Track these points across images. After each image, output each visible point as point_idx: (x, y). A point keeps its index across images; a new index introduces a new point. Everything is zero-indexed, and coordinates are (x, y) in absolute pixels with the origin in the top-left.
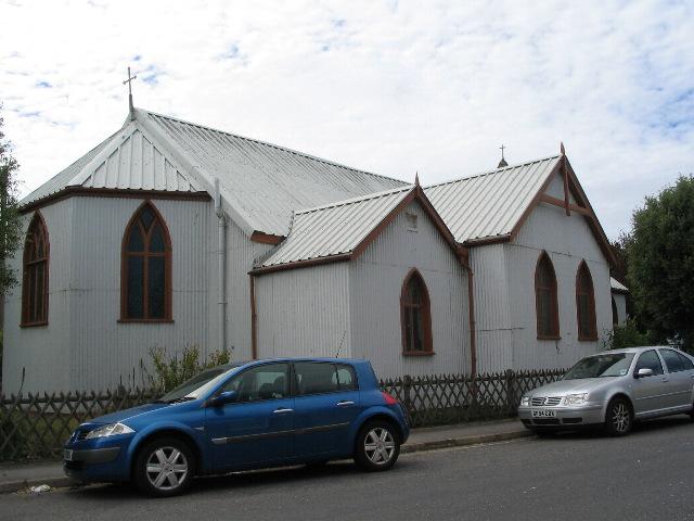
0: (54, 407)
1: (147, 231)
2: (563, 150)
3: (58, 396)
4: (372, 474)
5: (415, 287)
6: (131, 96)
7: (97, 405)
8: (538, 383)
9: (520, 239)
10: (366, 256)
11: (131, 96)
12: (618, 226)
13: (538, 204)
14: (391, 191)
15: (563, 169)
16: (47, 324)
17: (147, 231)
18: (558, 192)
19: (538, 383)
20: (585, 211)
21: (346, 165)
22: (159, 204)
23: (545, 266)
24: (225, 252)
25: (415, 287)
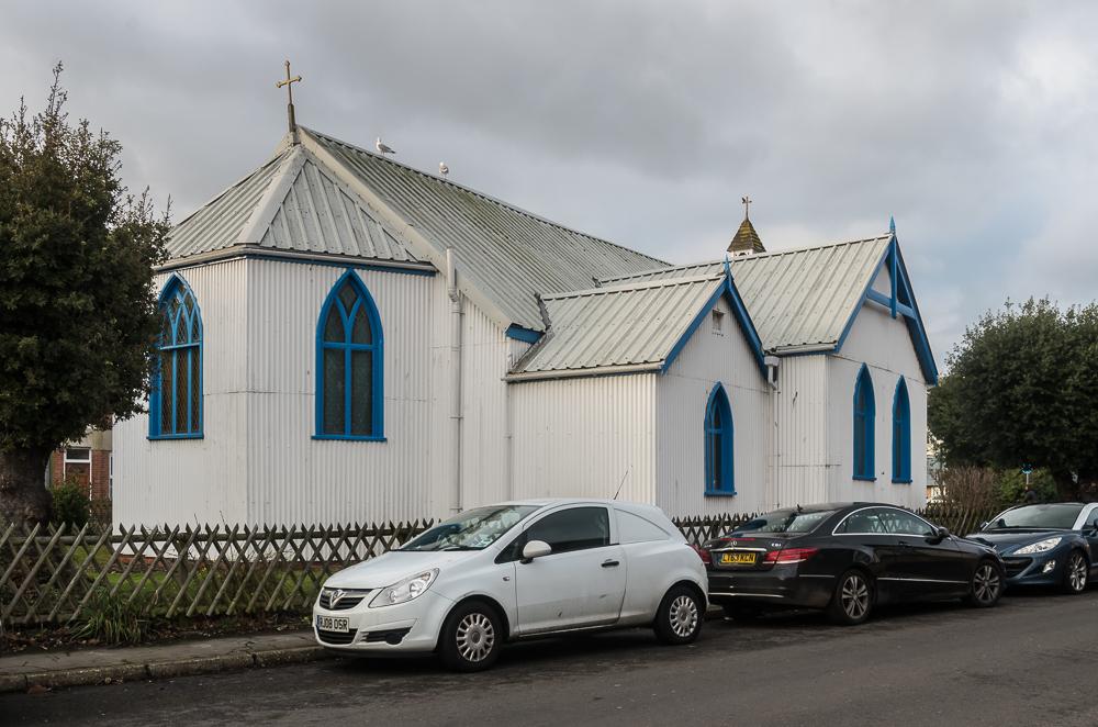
0: (134, 549)
1: (348, 315)
2: (893, 228)
3: (370, 528)
4: (777, 636)
5: (720, 407)
6: (291, 107)
7: (270, 545)
8: (379, 546)
9: (843, 352)
10: (673, 368)
11: (291, 107)
12: (949, 342)
13: (333, 305)
14: (632, 275)
15: (892, 261)
16: (203, 438)
17: (348, 315)
18: (885, 289)
19: (379, 546)
20: (910, 312)
21: (589, 234)
22: (358, 272)
23: (865, 381)
24: (459, 349)
25: (720, 407)
